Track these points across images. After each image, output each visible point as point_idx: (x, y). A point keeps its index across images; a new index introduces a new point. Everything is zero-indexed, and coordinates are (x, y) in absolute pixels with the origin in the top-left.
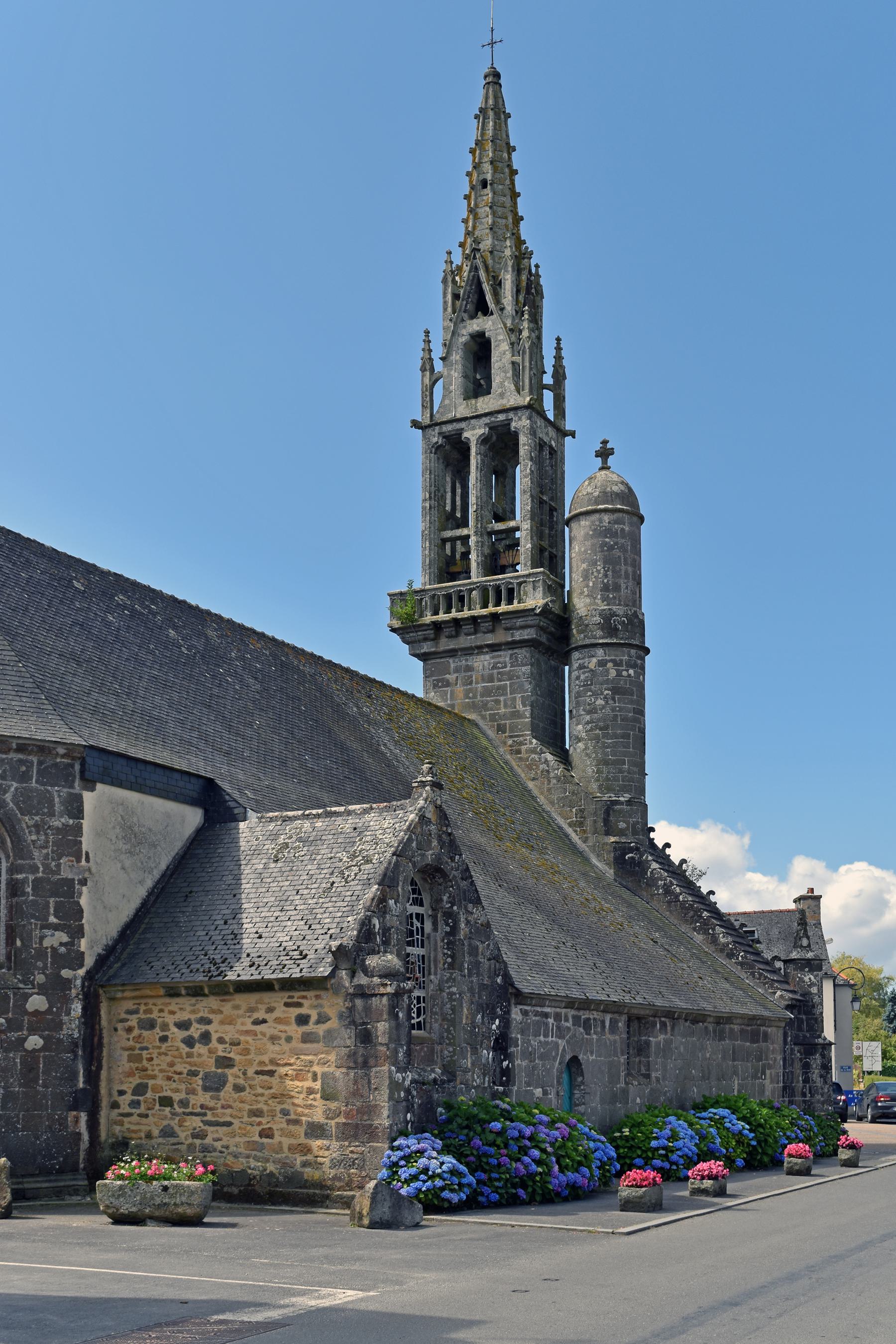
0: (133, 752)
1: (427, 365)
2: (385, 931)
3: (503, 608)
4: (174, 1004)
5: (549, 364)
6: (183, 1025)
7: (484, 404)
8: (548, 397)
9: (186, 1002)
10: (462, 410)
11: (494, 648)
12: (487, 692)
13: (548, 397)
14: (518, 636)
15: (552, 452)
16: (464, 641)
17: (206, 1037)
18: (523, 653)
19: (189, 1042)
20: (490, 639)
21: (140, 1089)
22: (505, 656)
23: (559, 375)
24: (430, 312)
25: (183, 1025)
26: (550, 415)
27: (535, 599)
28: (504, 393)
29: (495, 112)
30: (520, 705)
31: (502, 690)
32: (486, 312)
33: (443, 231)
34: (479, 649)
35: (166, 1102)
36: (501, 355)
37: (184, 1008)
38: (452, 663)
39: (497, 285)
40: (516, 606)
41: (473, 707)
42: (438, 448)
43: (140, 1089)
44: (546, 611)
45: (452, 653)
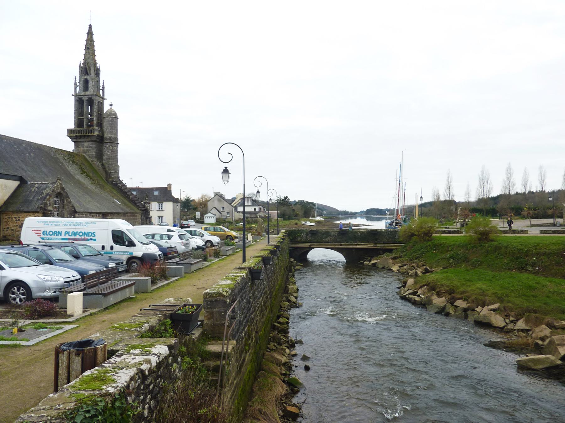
0: (6, 173)
1: (75, 83)
2: (50, 203)
3: (90, 134)
4: (14, 214)
5: (101, 85)
6: (15, 218)
7: (87, 93)
8: (101, 91)
9: (16, 214)
10: (83, 93)
11: (88, 141)
12: (87, 150)
13: (101, 91)
14: (93, 139)
15: (101, 103)
16: (82, 140)
17: (19, 220)
18: (94, 143)
19: (16, 220)
20: (87, 140)
21: (8, 228)
22: (91, 143)
23: (103, 87)
24: (76, 73)
25: (15, 218)
26: (102, 95)
27: (96, 133)
28: (91, 91)
29: (90, 33)
30: (93, 152)
31: (90, 150)
32: (88, 74)
33: (79, 57)
34: (86, 141)
35: (12, 230)
36: (91, 84)
37: (15, 215)
38: (80, 144)
39: (90, 69)
40: (92, 134)
41: (84, 152)
42: (78, 101)
43: (8, 228)
44: (98, 136)
45: (80, 142)
